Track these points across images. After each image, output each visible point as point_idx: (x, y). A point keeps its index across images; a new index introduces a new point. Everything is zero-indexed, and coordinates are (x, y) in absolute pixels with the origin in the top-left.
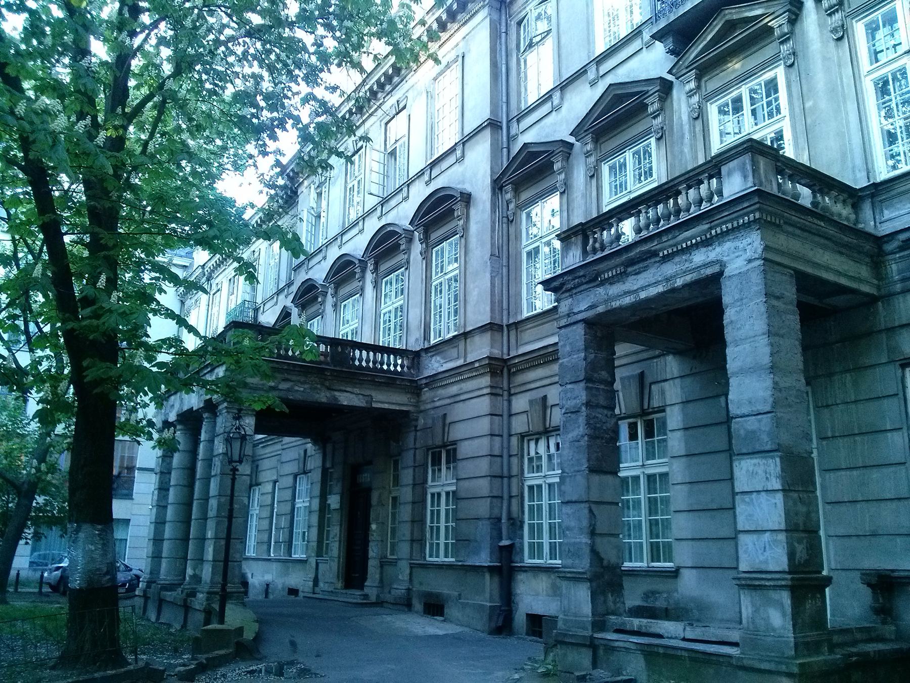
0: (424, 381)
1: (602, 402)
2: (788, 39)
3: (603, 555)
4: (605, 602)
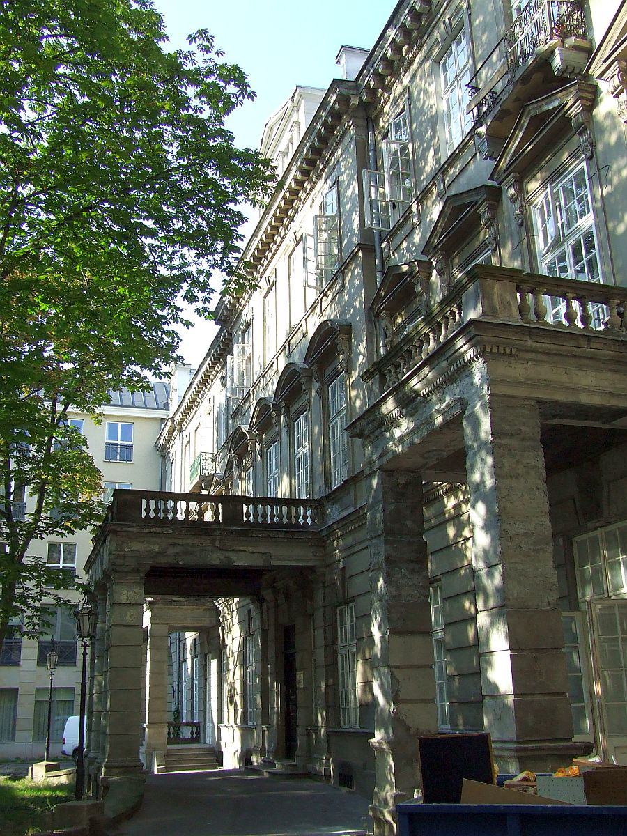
0: (325, 533)
2: (585, 129)
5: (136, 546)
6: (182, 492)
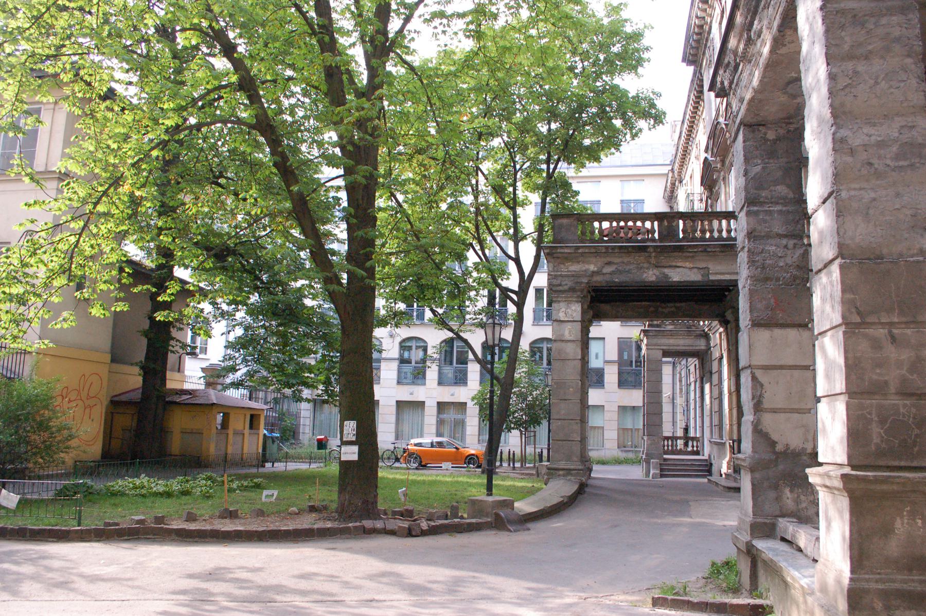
1: (778, 227)
3: (775, 437)
4: (778, 499)
5: (575, 268)
6: (625, 212)
